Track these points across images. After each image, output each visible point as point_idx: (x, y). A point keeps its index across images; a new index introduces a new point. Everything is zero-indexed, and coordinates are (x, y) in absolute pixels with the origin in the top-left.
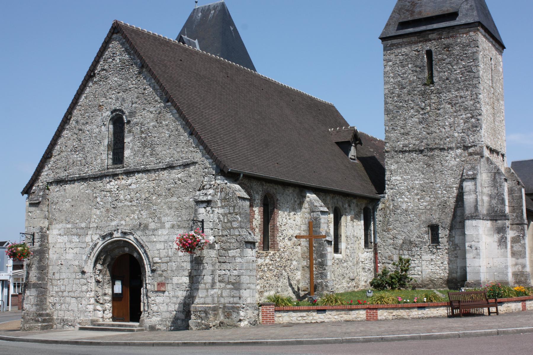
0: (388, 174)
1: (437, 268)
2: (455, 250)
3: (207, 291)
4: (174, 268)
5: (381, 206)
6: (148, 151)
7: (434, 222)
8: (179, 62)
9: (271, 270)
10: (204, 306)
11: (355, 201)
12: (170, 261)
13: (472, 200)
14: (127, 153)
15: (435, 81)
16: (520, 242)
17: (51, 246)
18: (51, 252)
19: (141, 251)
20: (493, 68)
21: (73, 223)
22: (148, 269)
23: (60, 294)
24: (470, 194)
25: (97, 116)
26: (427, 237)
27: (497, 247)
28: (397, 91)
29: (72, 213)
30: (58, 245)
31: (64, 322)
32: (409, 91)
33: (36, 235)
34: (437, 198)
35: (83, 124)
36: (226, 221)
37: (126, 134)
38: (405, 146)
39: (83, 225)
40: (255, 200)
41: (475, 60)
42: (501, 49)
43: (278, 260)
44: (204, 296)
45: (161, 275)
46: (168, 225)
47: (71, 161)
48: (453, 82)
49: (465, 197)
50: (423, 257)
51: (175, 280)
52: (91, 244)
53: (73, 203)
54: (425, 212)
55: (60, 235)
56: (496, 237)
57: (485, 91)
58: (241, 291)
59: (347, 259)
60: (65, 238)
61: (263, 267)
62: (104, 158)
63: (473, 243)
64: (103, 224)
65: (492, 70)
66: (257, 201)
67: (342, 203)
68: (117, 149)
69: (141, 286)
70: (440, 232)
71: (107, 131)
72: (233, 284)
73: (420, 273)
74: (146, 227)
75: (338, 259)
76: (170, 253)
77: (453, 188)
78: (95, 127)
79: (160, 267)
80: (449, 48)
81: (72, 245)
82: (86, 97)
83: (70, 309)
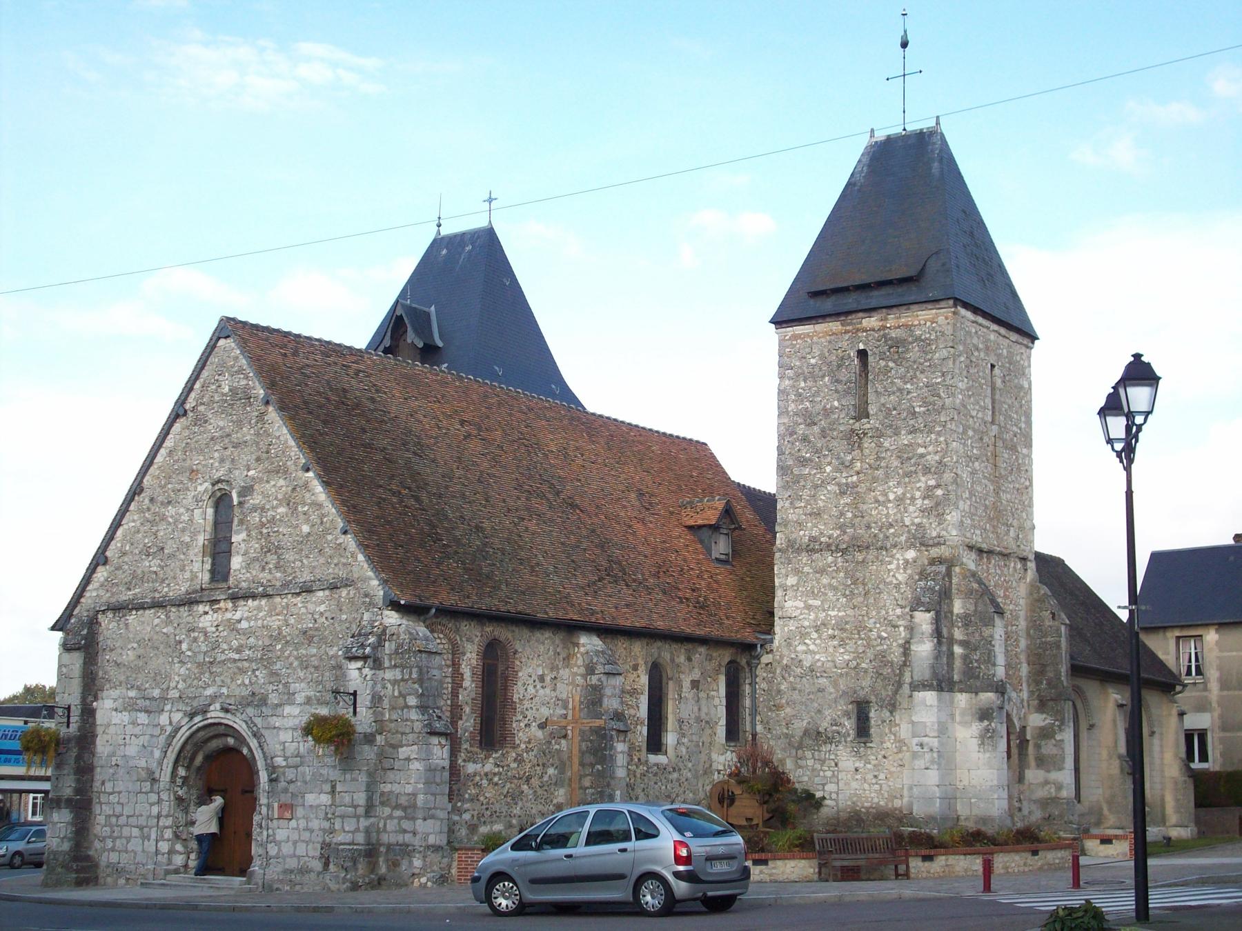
0: (779, 593)
1: (866, 786)
2: (900, 751)
4: (308, 778)
5: (766, 659)
7: (862, 693)
9: (496, 784)
12: (302, 764)
14: (236, 562)
15: (871, 412)
16: (1053, 737)
17: (99, 730)
18: (99, 741)
19: (253, 743)
20: (999, 383)
21: (139, 689)
22: (263, 776)
23: (114, 820)
25: (187, 489)
26: (849, 725)
27: (977, 748)
28: (801, 429)
29: (138, 670)
30: (112, 730)
31: (118, 871)
32: (823, 431)
33: (73, 708)
35: (162, 503)
36: (396, 694)
37: (234, 528)
38: (813, 539)
39: (156, 693)
40: (464, 654)
42: (1026, 341)
43: (514, 765)
45: (286, 790)
46: (300, 698)
47: (139, 572)
51: (311, 798)
52: (169, 729)
53: (141, 651)
54: (847, 674)
55: (116, 710)
57: (970, 433)
59: (681, 764)
60: (125, 717)
61: (478, 778)
62: (200, 569)
64: (191, 692)
65: (993, 389)
66: (468, 655)
67: (672, 653)
68: (219, 550)
70: (872, 714)
71: (204, 516)
72: (405, 809)
73: (834, 796)
74: (264, 701)
75: (657, 765)
77: (898, 627)
78: (182, 510)
79: (284, 773)
81: (137, 730)
82: (170, 453)
83: (130, 848)
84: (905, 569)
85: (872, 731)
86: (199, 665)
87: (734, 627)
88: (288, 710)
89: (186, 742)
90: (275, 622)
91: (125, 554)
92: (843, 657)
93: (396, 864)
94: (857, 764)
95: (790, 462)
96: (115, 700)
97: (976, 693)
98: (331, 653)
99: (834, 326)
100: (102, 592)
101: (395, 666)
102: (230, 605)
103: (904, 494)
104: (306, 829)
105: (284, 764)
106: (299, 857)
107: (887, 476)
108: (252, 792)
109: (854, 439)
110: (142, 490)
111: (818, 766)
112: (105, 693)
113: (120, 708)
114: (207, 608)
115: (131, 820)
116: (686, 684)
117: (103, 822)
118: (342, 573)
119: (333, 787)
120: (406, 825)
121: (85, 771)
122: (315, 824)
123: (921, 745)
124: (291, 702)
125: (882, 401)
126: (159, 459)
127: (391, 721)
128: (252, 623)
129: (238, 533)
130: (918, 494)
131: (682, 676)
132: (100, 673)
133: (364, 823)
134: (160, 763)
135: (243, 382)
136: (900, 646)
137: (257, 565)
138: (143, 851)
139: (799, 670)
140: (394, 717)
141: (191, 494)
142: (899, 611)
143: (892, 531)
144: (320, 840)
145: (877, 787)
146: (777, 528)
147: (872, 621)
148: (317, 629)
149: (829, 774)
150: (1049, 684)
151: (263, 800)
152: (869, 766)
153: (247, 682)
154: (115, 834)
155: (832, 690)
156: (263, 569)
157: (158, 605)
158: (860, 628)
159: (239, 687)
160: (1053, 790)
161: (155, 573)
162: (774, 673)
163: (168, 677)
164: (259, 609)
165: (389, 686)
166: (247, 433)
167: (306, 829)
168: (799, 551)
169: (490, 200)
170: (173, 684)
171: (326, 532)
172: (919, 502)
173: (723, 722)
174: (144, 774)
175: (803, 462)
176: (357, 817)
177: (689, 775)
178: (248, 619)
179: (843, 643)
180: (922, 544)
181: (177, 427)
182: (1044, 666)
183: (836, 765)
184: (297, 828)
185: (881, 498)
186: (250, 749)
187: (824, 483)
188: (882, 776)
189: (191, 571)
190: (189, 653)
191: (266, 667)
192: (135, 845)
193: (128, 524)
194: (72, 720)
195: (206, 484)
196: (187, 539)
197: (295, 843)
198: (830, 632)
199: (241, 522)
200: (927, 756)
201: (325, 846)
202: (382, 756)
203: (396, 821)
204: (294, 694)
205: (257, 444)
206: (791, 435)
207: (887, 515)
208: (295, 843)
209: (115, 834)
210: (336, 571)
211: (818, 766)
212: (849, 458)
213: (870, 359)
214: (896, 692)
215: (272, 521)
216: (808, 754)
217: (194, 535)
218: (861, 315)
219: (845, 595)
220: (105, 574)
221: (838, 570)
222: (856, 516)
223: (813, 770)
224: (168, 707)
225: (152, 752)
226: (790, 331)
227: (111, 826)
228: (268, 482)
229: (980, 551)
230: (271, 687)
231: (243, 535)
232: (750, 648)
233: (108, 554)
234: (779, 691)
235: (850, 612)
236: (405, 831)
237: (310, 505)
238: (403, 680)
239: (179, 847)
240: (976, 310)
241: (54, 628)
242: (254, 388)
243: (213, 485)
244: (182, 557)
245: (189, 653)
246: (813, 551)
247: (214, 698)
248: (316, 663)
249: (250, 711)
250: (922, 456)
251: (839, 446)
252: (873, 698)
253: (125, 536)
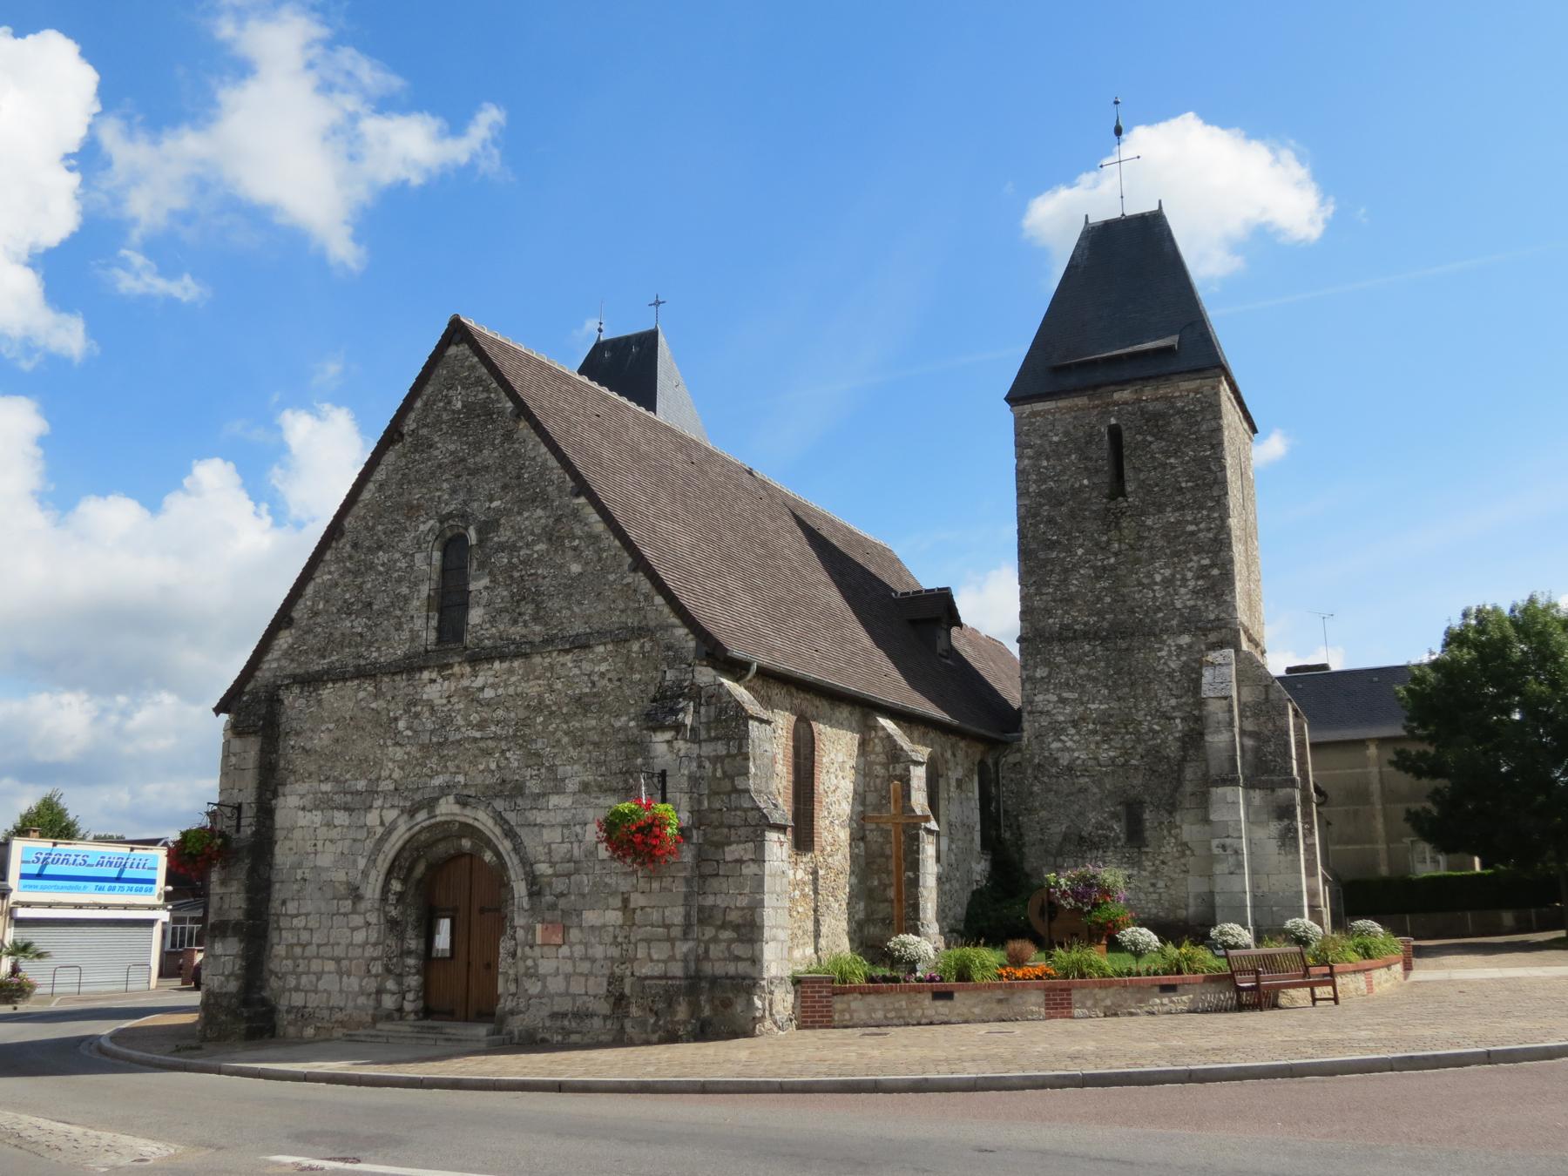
1: (1142, 896)
2: (1183, 855)
3: (673, 946)
4: (586, 890)
6: (528, 609)
8: (595, 418)
10: (663, 982)
11: (962, 744)
12: (577, 871)
14: (475, 615)
17: (280, 835)
18: (278, 849)
19: (505, 846)
21: (336, 780)
22: (520, 888)
23: (298, 950)
24: (1217, 731)
30: (297, 834)
32: (1072, 511)
33: (245, 807)
34: (1138, 741)
35: (369, 549)
36: (719, 774)
39: (361, 785)
44: (664, 957)
45: (553, 907)
46: (572, 785)
47: (337, 634)
48: (1169, 492)
49: (1208, 738)
51: (590, 917)
52: (380, 831)
53: (339, 734)
54: (1113, 772)
55: (303, 809)
56: (1274, 828)
60: (317, 817)
63: (1228, 841)
68: (450, 603)
69: (502, 932)
70: (1147, 816)
71: (428, 563)
72: (737, 928)
74: (518, 789)
76: (576, 852)
78: (397, 555)
79: (550, 884)
81: (334, 834)
84: (1178, 656)
85: (1147, 834)
86: (423, 747)
88: (554, 800)
89: (403, 848)
90: (533, 689)
91: (316, 614)
92: (1105, 754)
93: (727, 1004)
95: (1034, 546)
96: (302, 796)
97: (1273, 790)
98: (618, 724)
99: (1081, 401)
100: (284, 663)
101: (717, 739)
102: (468, 669)
103: (1173, 575)
104: (585, 958)
105: (550, 871)
106: (574, 996)
107: (1153, 559)
108: (498, 910)
109: (1111, 520)
110: (342, 534)
112: (288, 789)
113: (309, 806)
114: (434, 675)
115: (322, 950)
116: (953, 783)
117: (283, 953)
118: (632, 621)
119: (626, 901)
120: (738, 949)
121: (260, 890)
122: (598, 951)
123: (1224, 847)
124: (559, 791)
125: (1142, 476)
126: (366, 495)
127: (712, 810)
128: (500, 691)
129: (477, 578)
130: (1189, 575)
132: (282, 763)
133: (683, 948)
134: (365, 874)
135: (482, 396)
136: (1176, 739)
137: (506, 617)
138: (341, 991)
140: (717, 805)
141: (409, 536)
142: (1173, 702)
144: (607, 972)
145: (1155, 896)
148: (596, 695)
151: (519, 921)
153: (493, 766)
154: (300, 969)
156: (515, 622)
157: (364, 673)
158: (1127, 721)
159: (482, 772)
161: (361, 635)
163: (378, 763)
164: (511, 671)
165: (707, 764)
166: (488, 456)
167: (585, 958)
168: (1049, 640)
169: (657, 303)
170: (384, 774)
171: (605, 570)
172: (1191, 584)
173: (978, 827)
174: (342, 890)
175: (1052, 545)
176: (671, 940)
178: (494, 686)
179: (1106, 739)
180: (1197, 628)
181: (390, 457)
184: (571, 958)
185: (1146, 581)
186: (498, 854)
187: (1075, 567)
188: (1161, 884)
189: (411, 630)
190: (409, 733)
191: (521, 746)
192: (329, 983)
193: (322, 577)
194: (244, 822)
195: (431, 522)
196: (405, 590)
197: (568, 977)
198: (1091, 726)
199: (482, 565)
201: (614, 980)
202: (700, 859)
203: (724, 945)
204: (563, 780)
205: (504, 469)
206: (1034, 516)
207: (1154, 598)
208: (568, 977)
209: (300, 969)
210: (623, 619)
212: (1104, 538)
214: (1176, 789)
215: (526, 562)
217: (414, 585)
219: (1106, 686)
220: (290, 640)
221: (1097, 660)
224: (378, 803)
225: (355, 861)
226: (1027, 408)
227: (295, 959)
228: (520, 513)
230: (529, 772)
231: (485, 581)
233: (295, 615)
234: (1031, 793)
236: (738, 959)
237: (580, 538)
238: (728, 755)
239: (391, 985)
241: (218, 710)
242: (498, 401)
243: (441, 522)
244: (398, 613)
245: (409, 733)
246: (1067, 639)
247: (445, 790)
248: (596, 738)
249: (499, 804)
250: (1193, 533)
252: (1147, 798)
253: (317, 592)
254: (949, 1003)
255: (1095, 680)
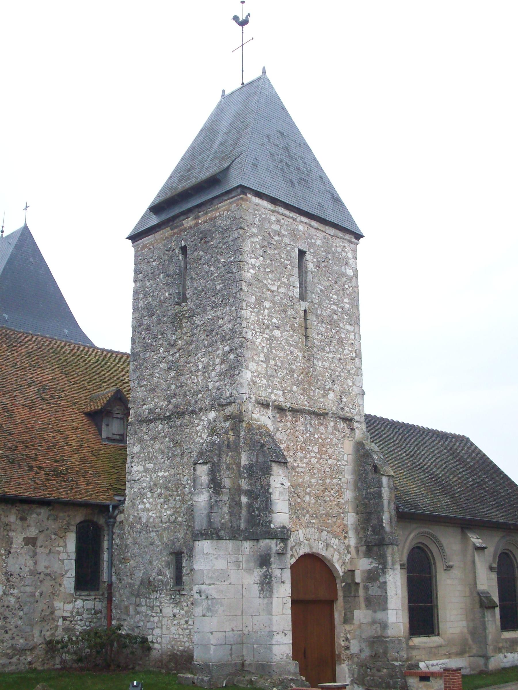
1: (180, 631)
13: (203, 504)
15: (188, 296)
16: (378, 579)
26: (169, 574)
41: (239, 251)
50: (164, 610)
54: (169, 527)
56: (257, 574)
58: (274, 628)
63: (203, 587)
80: (206, 238)
87: (87, 491)
94: (175, 611)
97: (258, 540)
103: (208, 363)
111: (149, 612)
123: (200, 593)
131: (11, 534)
139: (138, 526)
143: (200, 395)
146: (130, 406)
147: (186, 478)
149: (156, 619)
150: (373, 531)
152: (182, 612)
155: (159, 543)
160: (378, 629)
162: (124, 530)
172: (218, 367)
177: (19, 622)
182: (369, 514)
183: (161, 611)
185: (193, 369)
200: (204, 603)
211: (149, 612)
213: (188, 252)
216: (143, 601)
218: (182, 218)
222: (177, 387)
223: (147, 615)
229: (280, 409)
232: (103, 509)
235: (172, 472)
240: (274, 201)
251: (168, 328)
252: (185, 549)
254: (428, 683)
255: (163, 452)
